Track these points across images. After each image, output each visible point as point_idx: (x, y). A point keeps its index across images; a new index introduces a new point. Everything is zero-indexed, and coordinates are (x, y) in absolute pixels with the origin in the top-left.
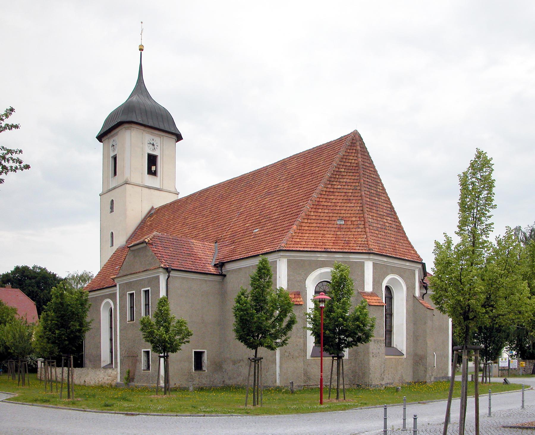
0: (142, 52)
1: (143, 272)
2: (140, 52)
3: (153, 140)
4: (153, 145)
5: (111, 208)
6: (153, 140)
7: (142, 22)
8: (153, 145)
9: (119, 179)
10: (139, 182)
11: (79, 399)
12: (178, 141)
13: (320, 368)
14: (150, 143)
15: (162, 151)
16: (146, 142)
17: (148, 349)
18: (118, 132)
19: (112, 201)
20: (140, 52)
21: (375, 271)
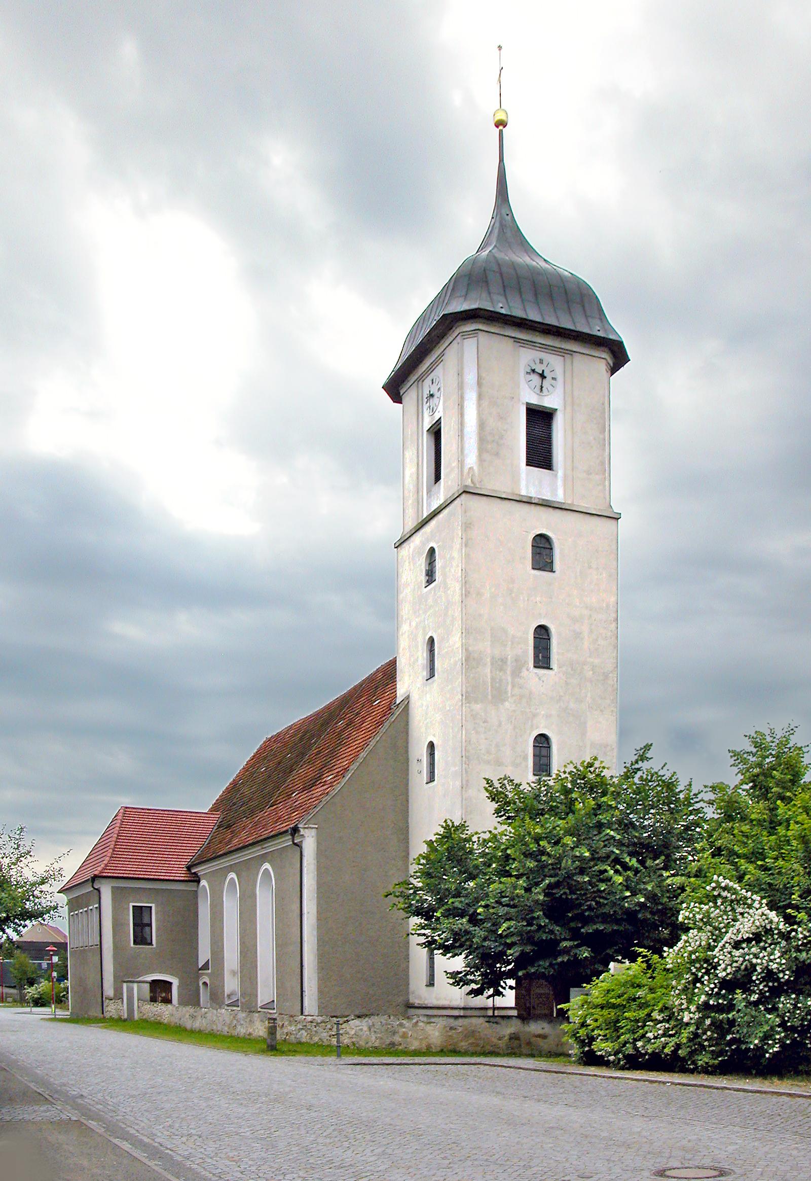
0: (504, 130)
1: (577, 352)
2: (497, 130)
3: (541, 361)
4: (542, 376)
5: (427, 575)
6: (541, 361)
7: (500, 48)
8: (542, 376)
9: (449, 483)
10: (503, 489)
11: (748, 831)
12: (614, 370)
13: (300, 981)
14: (533, 371)
15: (570, 400)
16: (522, 368)
17: (129, 908)
18: (442, 354)
19: (432, 551)
20: (497, 130)
21: (677, 1070)
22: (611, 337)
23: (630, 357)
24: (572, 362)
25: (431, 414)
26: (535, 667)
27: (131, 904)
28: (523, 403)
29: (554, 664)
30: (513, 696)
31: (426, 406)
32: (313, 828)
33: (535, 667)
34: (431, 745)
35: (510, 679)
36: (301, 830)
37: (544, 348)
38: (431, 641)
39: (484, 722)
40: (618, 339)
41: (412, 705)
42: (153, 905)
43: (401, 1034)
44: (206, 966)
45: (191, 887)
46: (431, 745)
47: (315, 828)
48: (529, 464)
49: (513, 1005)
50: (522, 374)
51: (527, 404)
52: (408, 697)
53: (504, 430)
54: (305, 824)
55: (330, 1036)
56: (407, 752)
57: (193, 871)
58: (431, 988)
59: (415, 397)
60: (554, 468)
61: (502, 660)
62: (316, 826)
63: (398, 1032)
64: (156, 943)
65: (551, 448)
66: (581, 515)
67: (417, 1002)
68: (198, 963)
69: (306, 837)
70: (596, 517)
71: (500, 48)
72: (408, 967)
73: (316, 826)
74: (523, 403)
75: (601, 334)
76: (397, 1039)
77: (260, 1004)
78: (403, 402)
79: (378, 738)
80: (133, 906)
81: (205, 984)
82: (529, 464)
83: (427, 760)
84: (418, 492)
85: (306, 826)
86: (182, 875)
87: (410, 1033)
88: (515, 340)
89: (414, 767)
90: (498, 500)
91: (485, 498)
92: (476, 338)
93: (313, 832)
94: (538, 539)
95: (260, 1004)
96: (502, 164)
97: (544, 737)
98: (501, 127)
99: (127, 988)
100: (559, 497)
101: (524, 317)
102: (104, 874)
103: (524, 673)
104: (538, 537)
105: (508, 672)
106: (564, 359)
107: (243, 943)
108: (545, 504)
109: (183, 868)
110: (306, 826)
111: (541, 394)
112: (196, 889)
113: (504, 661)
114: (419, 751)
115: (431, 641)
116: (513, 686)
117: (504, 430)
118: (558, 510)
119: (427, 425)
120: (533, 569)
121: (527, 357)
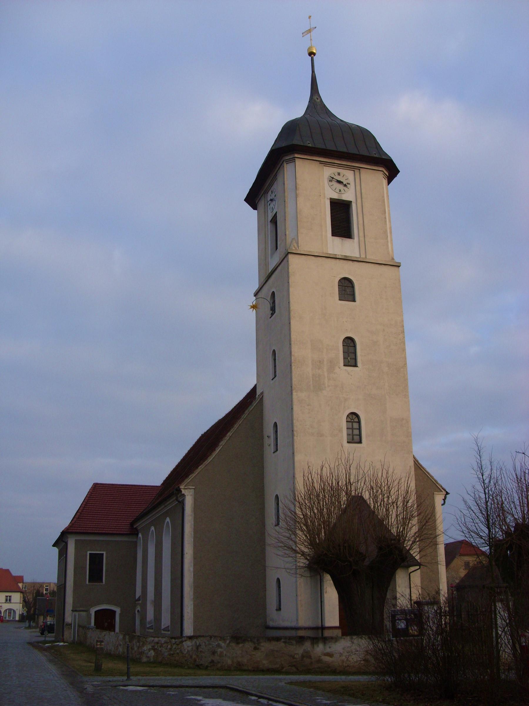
0: (314, 57)
17: (86, 555)
19: (273, 293)
22: (384, 157)
23: (400, 170)
24: (360, 174)
25: (272, 211)
26: (344, 365)
27: (89, 552)
28: (328, 199)
29: (359, 363)
30: (329, 386)
31: (269, 207)
32: (191, 489)
33: (344, 365)
34: (275, 425)
35: (326, 374)
36: (183, 491)
37: (340, 166)
38: (274, 351)
39: (308, 405)
40: (388, 158)
41: (264, 399)
42: (104, 553)
43: (219, 653)
44: (139, 599)
45: (132, 539)
46: (275, 425)
47: (193, 488)
48: (333, 235)
49: (337, 624)
50: (326, 182)
51: (331, 199)
52: (262, 393)
53: (315, 215)
54: (185, 486)
55: (170, 655)
56: (262, 431)
57: (135, 527)
58: (279, 612)
59: (263, 205)
60: (353, 237)
61: (320, 362)
62: (194, 487)
63: (217, 652)
64: (105, 581)
65: (349, 225)
66: (373, 265)
67: (271, 624)
68: (135, 595)
69: (186, 496)
70: (383, 266)
71: (310, 17)
72: (265, 596)
73: (194, 487)
74: (328, 199)
75: (377, 156)
76: (216, 658)
77: (163, 627)
78: (258, 209)
79: (241, 422)
80: (103, 554)
81: (138, 611)
82: (334, 234)
83: (274, 436)
84: (266, 259)
85: (186, 487)
86: (126, 530)
87: (225, 653)
88: (321, 162)
89: (266, 441)
90: (313, 258)
91: (303, 256)
92: (294, 163)
93: (192, 491)
94: (343, 281)
95: (163, 627)
96: (313, 74)
97: (355, 415)
98: (313, 56)
99: (79, 614)
100: (355, 254)
101: (325, 148)
102: (70, 531)
103: (337, 370)
104: (343, 280)
105: (325, 370)
106: (355, 173)
107: (156, 580)
108: (346, 259)
109: (128, 525)
110: (186, 487)
111: (340, 193)
112: (135, 540)
113: (321, 362)
114: (269, 430)
115: (274, 351)
116: (329, 379)
117: (315, 215)
118: (356, 263)
119: (270, 218)
120: (340, 300)
121: (329, 171)
